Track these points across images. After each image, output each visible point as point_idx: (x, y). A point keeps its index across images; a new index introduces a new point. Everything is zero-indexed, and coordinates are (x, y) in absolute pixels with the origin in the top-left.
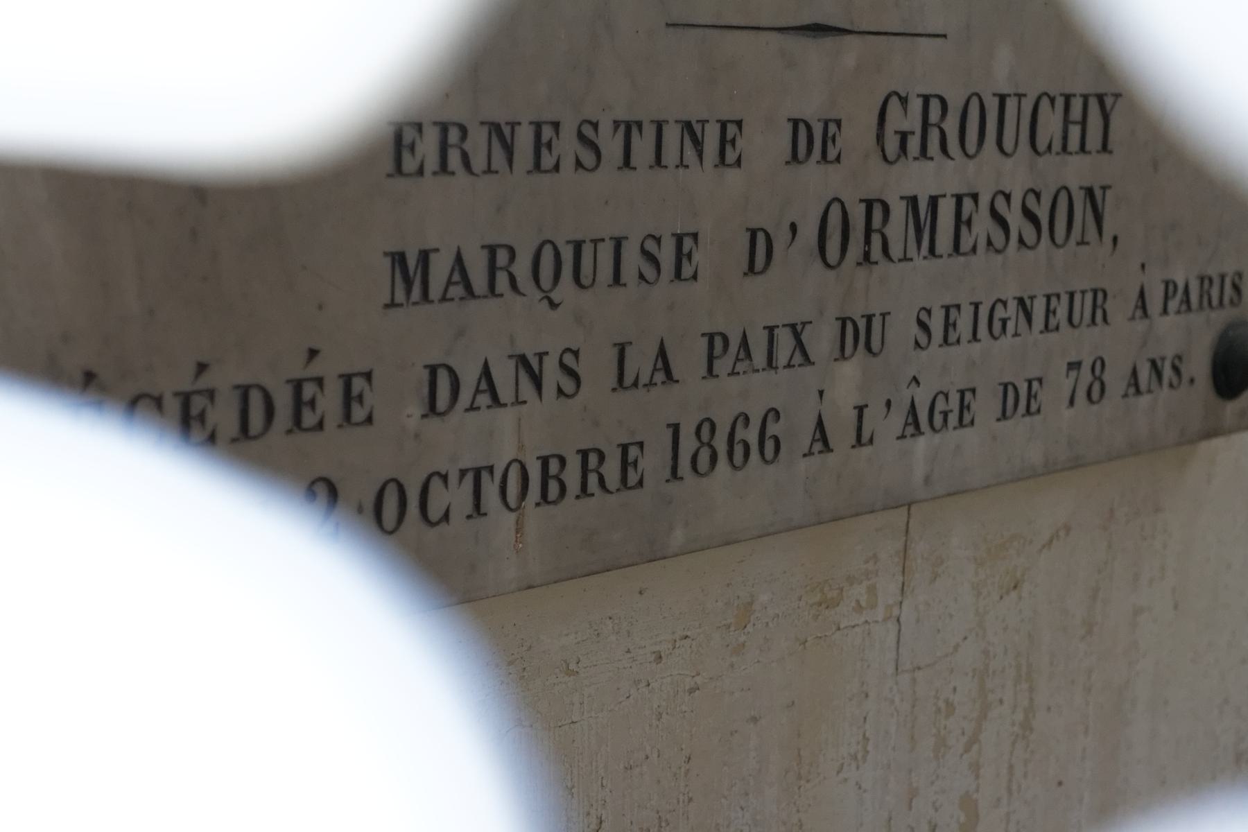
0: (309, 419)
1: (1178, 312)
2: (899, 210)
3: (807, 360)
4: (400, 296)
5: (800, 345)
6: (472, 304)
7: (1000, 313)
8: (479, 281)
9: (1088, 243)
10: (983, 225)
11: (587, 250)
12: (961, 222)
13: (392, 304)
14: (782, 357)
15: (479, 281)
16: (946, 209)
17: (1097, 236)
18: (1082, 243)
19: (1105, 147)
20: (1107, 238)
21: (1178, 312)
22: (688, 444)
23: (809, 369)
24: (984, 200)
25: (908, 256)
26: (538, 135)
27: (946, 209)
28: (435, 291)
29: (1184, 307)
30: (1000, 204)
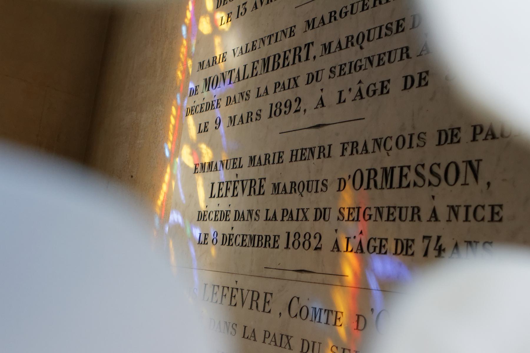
0: (391, 218)
1: (288, 220)
2: (380, 172)
3: (306, 220)
4: (274, 193)
5: (305, 216)
6: (287, 195)
7: (368, 212)
8: (288, 190)
9: (468, 184)
10: (412, 176)
11: (310, 183)
12: (402, 176)
13: (273, 194)
14: (300, 218)
15: (288, 190)
16: (397, 172)
17: (474, 179)
18: (465, 184)
19: (213, 184)
20: (482, 182)
21: (288, 220)
22: (292, 239)
23: (307, 222)
24: (427, 167)
25: (467, 183)
26: (452, 132)
27: (397, 172)
28: (280, 192)
29: (290, 219)
30: (420, 169)
